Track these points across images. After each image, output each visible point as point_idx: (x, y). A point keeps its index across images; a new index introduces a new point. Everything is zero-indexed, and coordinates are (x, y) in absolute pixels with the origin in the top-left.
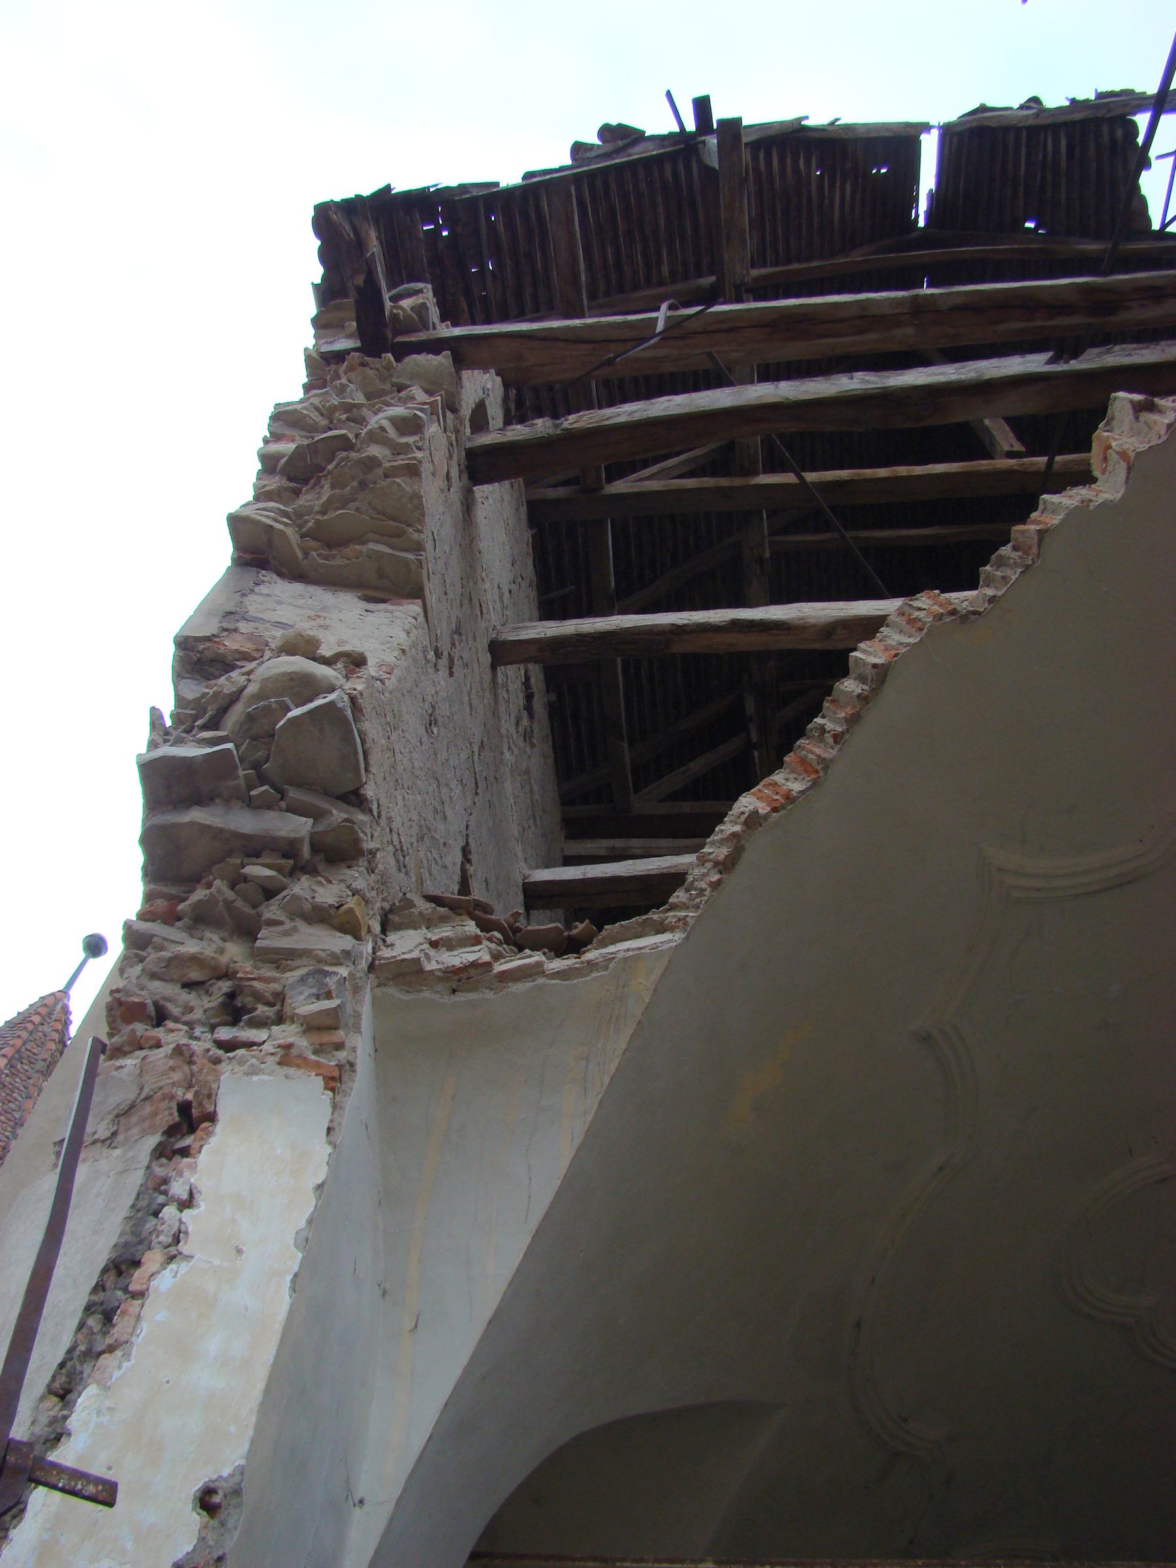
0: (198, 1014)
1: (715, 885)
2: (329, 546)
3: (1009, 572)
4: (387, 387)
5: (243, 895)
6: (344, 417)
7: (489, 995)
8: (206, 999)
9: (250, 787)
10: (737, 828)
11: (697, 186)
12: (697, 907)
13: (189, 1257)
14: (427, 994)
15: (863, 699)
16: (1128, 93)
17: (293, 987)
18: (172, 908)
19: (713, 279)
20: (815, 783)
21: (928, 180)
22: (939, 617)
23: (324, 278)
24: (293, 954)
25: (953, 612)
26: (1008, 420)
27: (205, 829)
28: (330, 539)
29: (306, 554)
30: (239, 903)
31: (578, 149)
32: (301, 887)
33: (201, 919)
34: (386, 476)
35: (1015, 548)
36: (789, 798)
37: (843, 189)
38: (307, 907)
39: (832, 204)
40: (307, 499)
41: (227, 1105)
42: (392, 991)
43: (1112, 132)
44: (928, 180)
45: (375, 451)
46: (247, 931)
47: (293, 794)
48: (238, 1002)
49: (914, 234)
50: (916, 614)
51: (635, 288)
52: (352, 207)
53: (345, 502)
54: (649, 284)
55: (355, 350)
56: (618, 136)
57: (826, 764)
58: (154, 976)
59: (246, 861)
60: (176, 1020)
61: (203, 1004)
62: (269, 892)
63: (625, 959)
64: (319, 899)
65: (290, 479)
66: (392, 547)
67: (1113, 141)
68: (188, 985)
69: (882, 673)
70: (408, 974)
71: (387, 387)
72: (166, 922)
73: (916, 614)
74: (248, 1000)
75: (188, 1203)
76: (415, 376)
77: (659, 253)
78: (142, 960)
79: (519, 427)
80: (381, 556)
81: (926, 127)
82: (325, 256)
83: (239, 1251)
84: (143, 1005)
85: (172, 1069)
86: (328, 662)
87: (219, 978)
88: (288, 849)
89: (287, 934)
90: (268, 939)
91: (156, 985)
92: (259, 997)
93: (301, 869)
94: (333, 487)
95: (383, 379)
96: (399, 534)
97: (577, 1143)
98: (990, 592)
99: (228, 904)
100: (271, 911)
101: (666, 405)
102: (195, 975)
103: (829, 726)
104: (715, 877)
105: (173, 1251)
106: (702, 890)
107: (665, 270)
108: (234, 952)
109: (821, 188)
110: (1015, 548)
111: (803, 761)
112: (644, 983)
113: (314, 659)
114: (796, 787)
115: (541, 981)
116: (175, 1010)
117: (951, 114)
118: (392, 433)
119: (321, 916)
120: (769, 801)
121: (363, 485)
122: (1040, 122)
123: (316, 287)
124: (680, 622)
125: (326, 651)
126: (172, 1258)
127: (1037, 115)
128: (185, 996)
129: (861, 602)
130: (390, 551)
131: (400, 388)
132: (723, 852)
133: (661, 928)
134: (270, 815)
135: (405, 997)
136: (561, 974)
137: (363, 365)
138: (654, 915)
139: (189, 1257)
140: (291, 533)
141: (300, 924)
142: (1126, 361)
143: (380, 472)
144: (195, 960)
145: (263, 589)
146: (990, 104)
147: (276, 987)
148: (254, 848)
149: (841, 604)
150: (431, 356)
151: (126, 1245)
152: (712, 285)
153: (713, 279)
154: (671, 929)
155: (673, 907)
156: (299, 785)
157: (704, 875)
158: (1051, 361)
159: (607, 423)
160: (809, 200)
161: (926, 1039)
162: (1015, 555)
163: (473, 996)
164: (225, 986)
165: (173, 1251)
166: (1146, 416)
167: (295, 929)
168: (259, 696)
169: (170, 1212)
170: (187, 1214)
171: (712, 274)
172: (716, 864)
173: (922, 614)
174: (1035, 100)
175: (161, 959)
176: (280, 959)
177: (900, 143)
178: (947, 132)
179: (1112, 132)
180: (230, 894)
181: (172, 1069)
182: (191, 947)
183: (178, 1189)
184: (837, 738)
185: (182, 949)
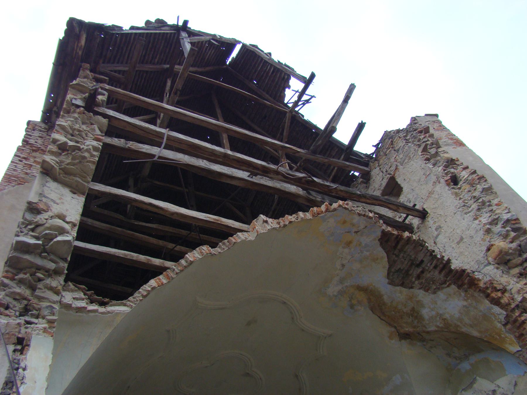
0: (17, 309)
1: (141, 300)
2: (66, 173)
3: (225, 247)
4: (88, 122)
5: (34, 280)
6: (77, 133)
7: (84, 315)
8: (19, 304)
9: (42, 253)
10: (149, 289)
11: (175, 40)
12: (135, 304)
13: (26, 383)
14: (71, 312)
15: (185, 267)
16: (293, 70)
17: (44, 308)
18: (14, 277)
19: (168, 66)
20: (169, 282)
21: (234, 54)
22: (207, 254)
23: (64, 38)
24: (43, 298)
25: (211, 253)
26: (228, 136)
27: (28, 261)
28: (66, 172)
29: (59, 174)
30: (32, 281)
31: (148, 22)
32: (48, 281)
33: (21, 282)
34: (87, 162)
35: (228, 242)
36: (162, 284)
37: (212, 51)
38: (49, 286)
39: (207, 54)
40: (63, 158)
41: (33, 343)
42: (63, 310)
43: (285, 75)
44: (234, 54)
45: (86, 155)
46: (33, 289)
47: (52, 257)
48: (28, 307)
49: (225, 67)
50: (203, 251)
51: (147, 63)
52: (81, 23)
53: (74, 165)
54: (150, 63)
55: (83, 107)
56: (161, 23)
57: (173, 278)
58: (7, 295)
59: (37, 271)
60: (11, 309)
61: (19, 306)
62: (40, 280)
63: (117, 313)
64: (52, 285)
65: (59, 149)
66: (82, 180)
67: (284, 78)
68: (15, 299)
69: (191, 262)
70: (68, 307)
71: (88, 122)
72: (11, 280)
73: (203, 251)
74: (31, 308)
75: (24, 369)
76: (98, 123)
77: (157, 55)
78: (5, 290)
79: (116, 139)
80: (79, 182)
81: (239, 42)
82: (66, 32)
83: (35, 382)
84: (5, 304)
85: (16, 328)
86: (68, 223)
87: (23, 299)
88: (47, 271)
89: (43, 292)
90: (38, 293)
91: (8, 298)
92: (34, 308)
93: (50, 276)
94: (72, 159)
95: (88, 119)
96: (85, 177)
97: (94, 351)
98: (219, 250)
99: (29, 281)
100: (40, 285)
101: (156, 150)
102: (18, 297)
103: (176, 270)
104: (141, 298)
105: (22, 381)
106: (137, 300)
107: (156, 60)
108: (27, 293)
109: (206, 49)
110: (228, 242)
111: (167, 275)
112: (119, 319)
113: (64, 221)
114: (165, 281)
115: (97, 314)
116: (11, 306)
117: (248, 42)
118: (92, 151)
119: (51, 289)
120: (158, 284)
121: (80, 162)
122: (269, 61)
123: (60, 40)
124: (137, 198)
125: (68, 219)
126: (22, 383)
127: (269, 59)
128: (15, 303)
129: (183, 209)
130: (81, 181)
131: (92, 124)
132: (145, 293)
133: (125, 305)
134: (45, 261)
135: (66, 312)
136: (102, 313)
137: (84, 113)
138: (124, 301)
139: (26, 383)
140: (58, 168)
141: (46, 290)
142: (265, 183)
143: (86, 160)
144: (19, 294)
145: (48, 184)
146: (259, 47)
147: (39, 306)
148: (39, 268)
149: (177, 207)
150: (103, 119)
151: (9, 377)
152: (167, 68)
153: (168, 66)
154: (128, 306)
155: (129, 301)
156: (53, 254)
157: (138, 297)
158: (249, 176)
159: (140, 150)
160: (202, 52)
161: (168, 331)
162: (228, 244)
163: (81, 314)
164: (25, 302)
165: (22, 381)
166: (265, 224)
167: (45, 292)
168: (49, 228)
169: (20, 370)
170: (25, 372)
171: (168, 64)
172: (142, 295)
173: (204, 252)
174: (270, 54)
175: (10, 291)
176: (41, 299)
177: (230, 45)
178: (244, 46)
179: (285, 75)
180: (30, 278)
181: (16, 328)
182: (18, 290)
183: (22, 365)
184: (177, 273)
185: (15, 290)
